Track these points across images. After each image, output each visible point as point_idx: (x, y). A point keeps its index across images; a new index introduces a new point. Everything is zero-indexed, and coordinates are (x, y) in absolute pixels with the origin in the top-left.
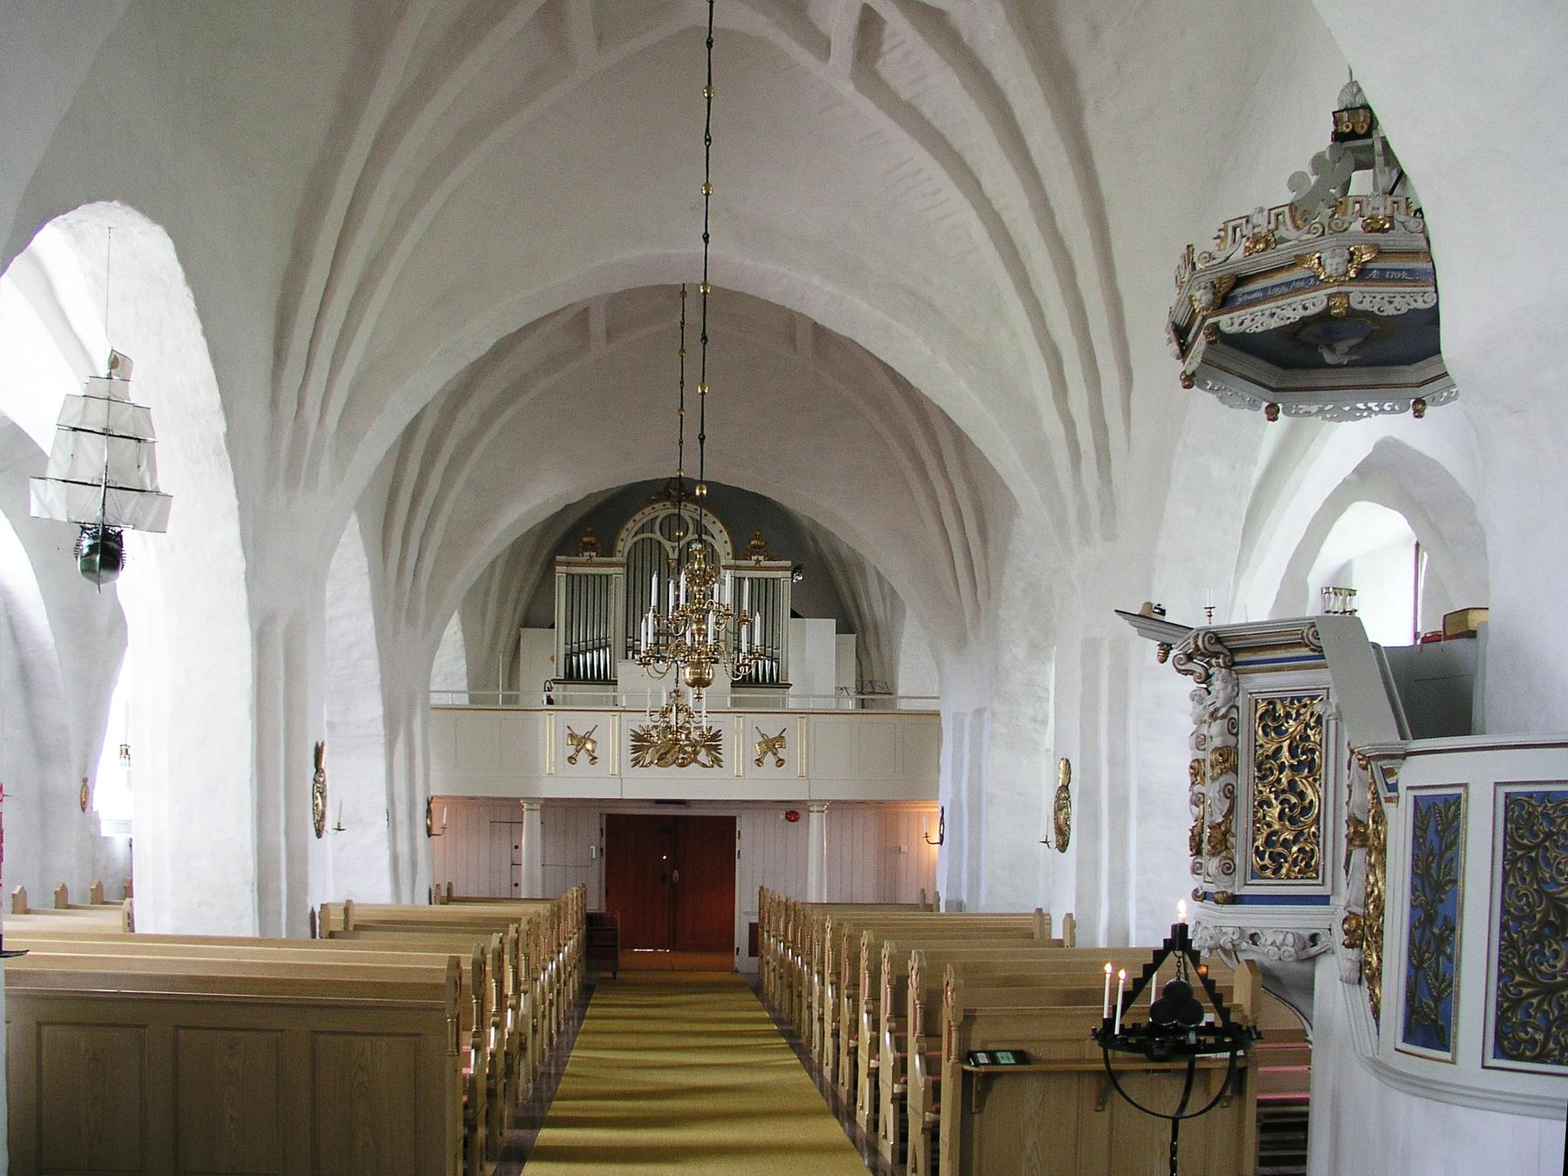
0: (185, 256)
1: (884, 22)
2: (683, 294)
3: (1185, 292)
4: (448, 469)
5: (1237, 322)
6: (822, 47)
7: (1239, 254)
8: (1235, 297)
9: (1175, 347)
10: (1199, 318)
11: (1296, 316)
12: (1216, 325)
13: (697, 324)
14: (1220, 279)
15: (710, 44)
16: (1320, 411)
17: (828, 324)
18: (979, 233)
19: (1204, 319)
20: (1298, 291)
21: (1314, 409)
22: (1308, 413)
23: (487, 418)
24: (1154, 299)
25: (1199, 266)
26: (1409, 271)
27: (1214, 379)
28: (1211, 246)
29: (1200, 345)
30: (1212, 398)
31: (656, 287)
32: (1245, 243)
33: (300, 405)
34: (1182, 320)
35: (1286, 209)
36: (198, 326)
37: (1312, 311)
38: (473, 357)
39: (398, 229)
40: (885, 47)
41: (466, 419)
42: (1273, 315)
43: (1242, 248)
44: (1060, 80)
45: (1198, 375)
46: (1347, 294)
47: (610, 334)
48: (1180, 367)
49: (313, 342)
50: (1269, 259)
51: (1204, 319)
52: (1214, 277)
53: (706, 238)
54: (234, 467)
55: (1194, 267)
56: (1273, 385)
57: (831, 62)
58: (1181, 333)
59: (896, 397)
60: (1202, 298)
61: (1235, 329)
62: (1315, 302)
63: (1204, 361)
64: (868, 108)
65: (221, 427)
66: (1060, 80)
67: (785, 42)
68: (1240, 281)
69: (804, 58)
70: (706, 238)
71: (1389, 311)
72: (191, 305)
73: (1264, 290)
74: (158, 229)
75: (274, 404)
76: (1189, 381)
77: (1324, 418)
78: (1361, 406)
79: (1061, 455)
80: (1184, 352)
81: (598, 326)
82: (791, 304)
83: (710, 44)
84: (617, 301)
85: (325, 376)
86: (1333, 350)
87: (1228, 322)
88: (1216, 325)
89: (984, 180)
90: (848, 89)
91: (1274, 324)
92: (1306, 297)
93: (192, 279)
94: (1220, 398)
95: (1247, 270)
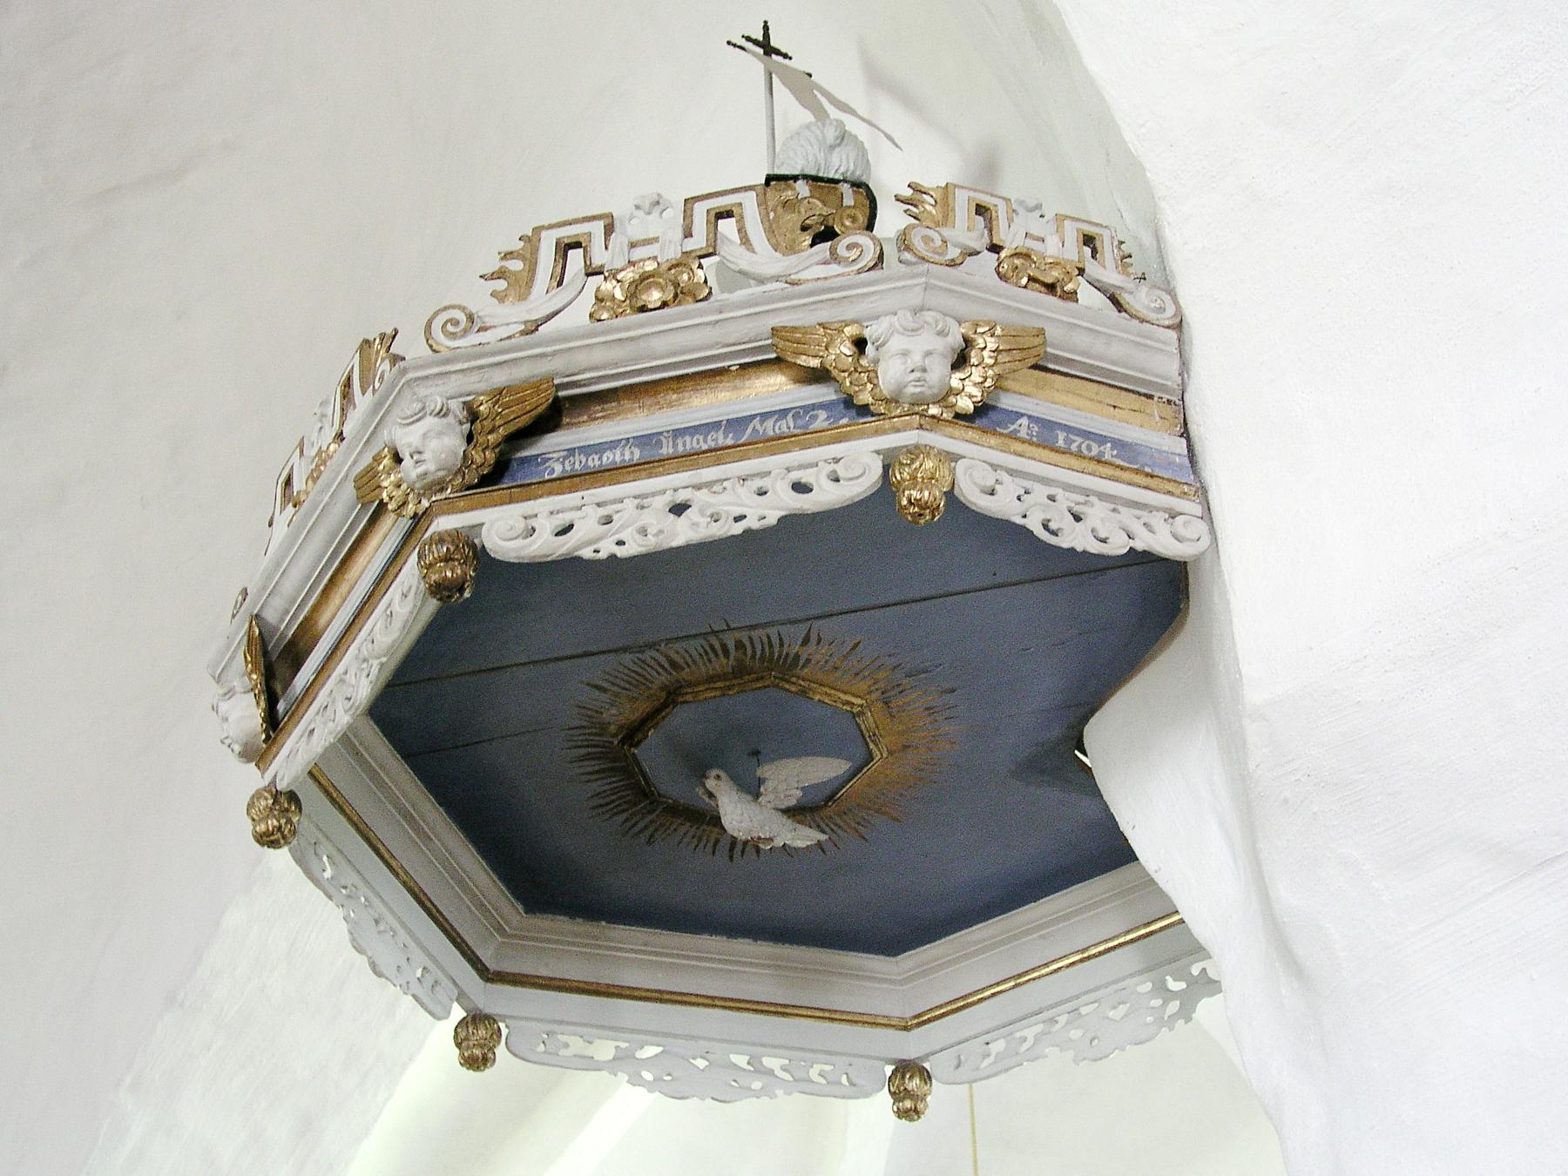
11: (764, 512)
16: (622, 1060)
20: (777, 443)
21: (605, 1050)
22: (588, 1064)
26: (1119, 444)
34: (282, 618)
35: (750, 202)
37: (826, 496)
42: (679, 509)
43: (587, 301)
46: (955, 458)
50: (673, 338)
56: (486, 956)
58: (278, 662)
60: (433, 445)
62: (844, 471)
68: (552, 417)
71: (1076, 538)
73: (644, 441)
76: (278, 822)
77: (636, 1080)
78: (741, 1060)
86: (752, 789)
91: (683, 532)
92: (812, 461)
95: (594, 363)
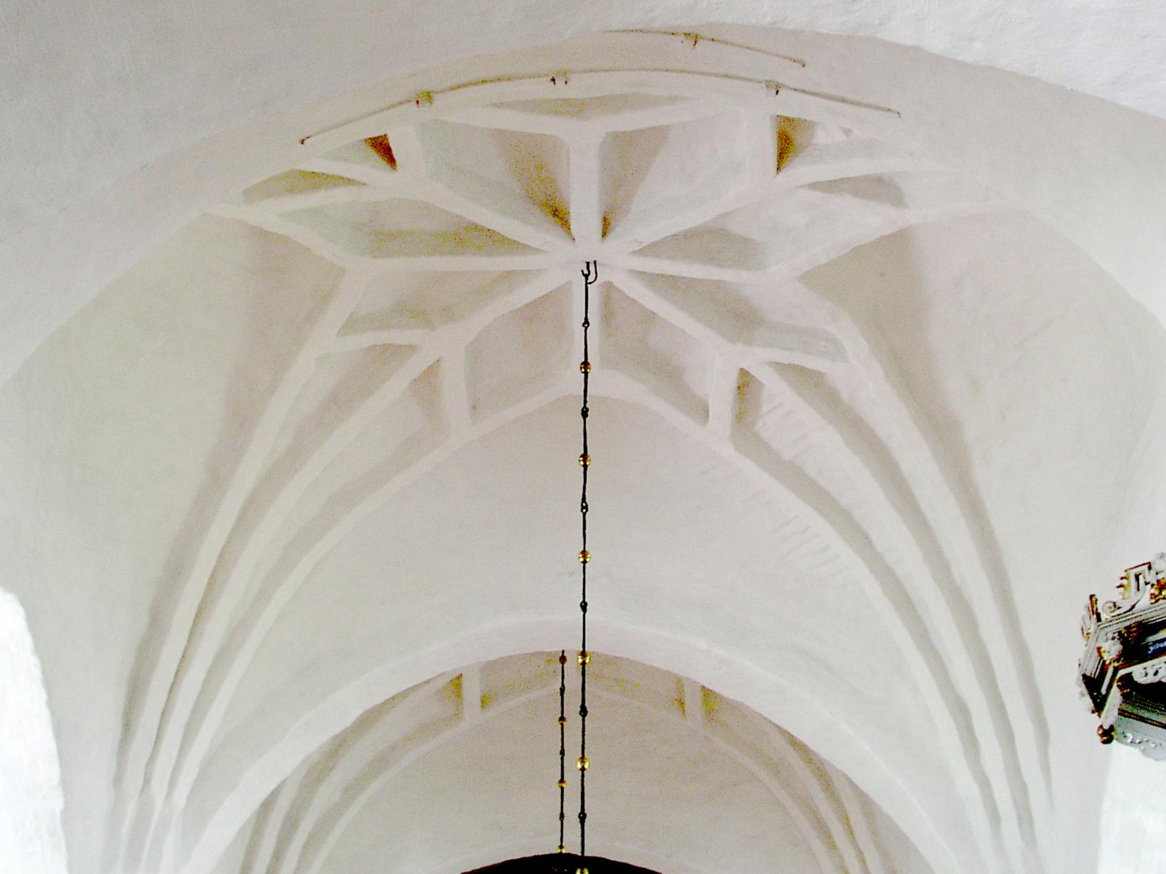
0: (34, 622)
1: (761, 384)
2: (563, 659)
3: (1094, 645)
4: (307, 846)
5: (1151, 672)
6: (702, 412)
7: (1144, 600)
8: (1147, 646)
9: (1088, 702)
10: (1110, 671)
12: (1129, 676)
13: (575, 685)
14: (1128, 628)
15: (585, 413)
17: (717, 689)
18: (873, 589)
19: (1116, 670)
23: (351, 791)
24: (1068, 651)
25: (1103, 616)
27: (1134, 731)
28: (1116, 595)
29: (1115, 698)
30: (1135, 750)
31: (533, 654)
32: (1149, 590)
33: (147, 780)
34: (1092, 669)
36: (43, 697)
38: (337, 730)
39: (263, 595)
40: (765, 409)
41: (328, 793)
43: (1147, 596)
44: (942, 431)
45: (1118, 730)
47: (485, 702)
48: (1095, 721)
49: (164, 714)
51: (1116, 670)
52: (1121, 626)
53: (584, 606)
54: (69, 848)
55: (1099, 619)
57: (710, 424)
58: (1093, 685)
59: (793, 758)
60: (1112, 649)
61: (1151, 679)
63: (1122, 713)
64: (748, 467)
65: (57, 803)
66: (942, 431)
67: (661, 407)
69: (682, 421)
70: (584, 606)
72: (37, 674)
74: (10, 597)
75: (118, 779)
79: (979, 820)
80: (1099, 706)
81: (472, 692)
82: (678, 669)
83: (585, 413)
84: (489, 669)
85: (176, 753)
87: (1142, 673)
88: (1129, 676)
89: (874, 535)
90: (728, 451)
93: (41, 648)
94: (1144, 751)
